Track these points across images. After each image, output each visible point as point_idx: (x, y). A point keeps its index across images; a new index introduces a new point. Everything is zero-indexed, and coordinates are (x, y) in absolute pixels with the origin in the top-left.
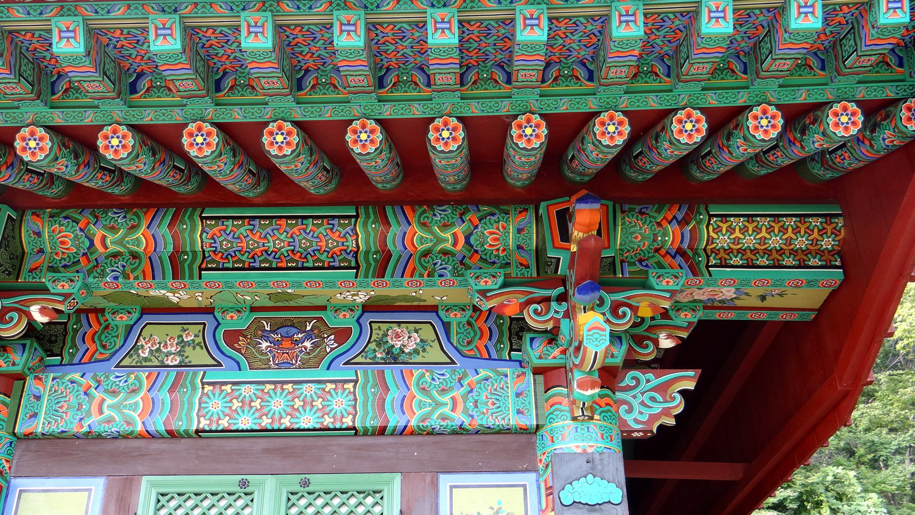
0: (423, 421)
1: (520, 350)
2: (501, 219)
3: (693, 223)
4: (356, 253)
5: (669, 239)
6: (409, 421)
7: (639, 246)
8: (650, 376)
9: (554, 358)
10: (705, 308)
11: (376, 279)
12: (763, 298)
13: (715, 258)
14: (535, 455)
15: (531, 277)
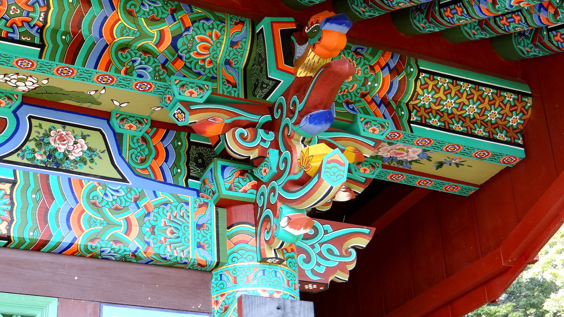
0: (92, 240)
1: (197, 179)
2: (216, 26)
3: (403, 74)
4: (42, 28)
5: (378, 86)
6: (75, 239)
7: (347, 87)
8: (328, 227)
9: (245, 191)
10: (384, 166)
11: (64, 65)
12: (440, 165)
13: (416, 115)
14: (209, 295)
15: (238, 98)
